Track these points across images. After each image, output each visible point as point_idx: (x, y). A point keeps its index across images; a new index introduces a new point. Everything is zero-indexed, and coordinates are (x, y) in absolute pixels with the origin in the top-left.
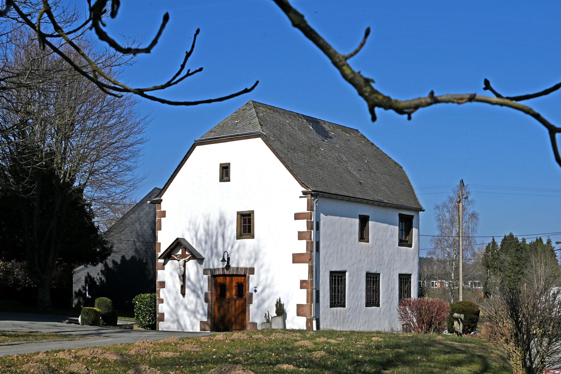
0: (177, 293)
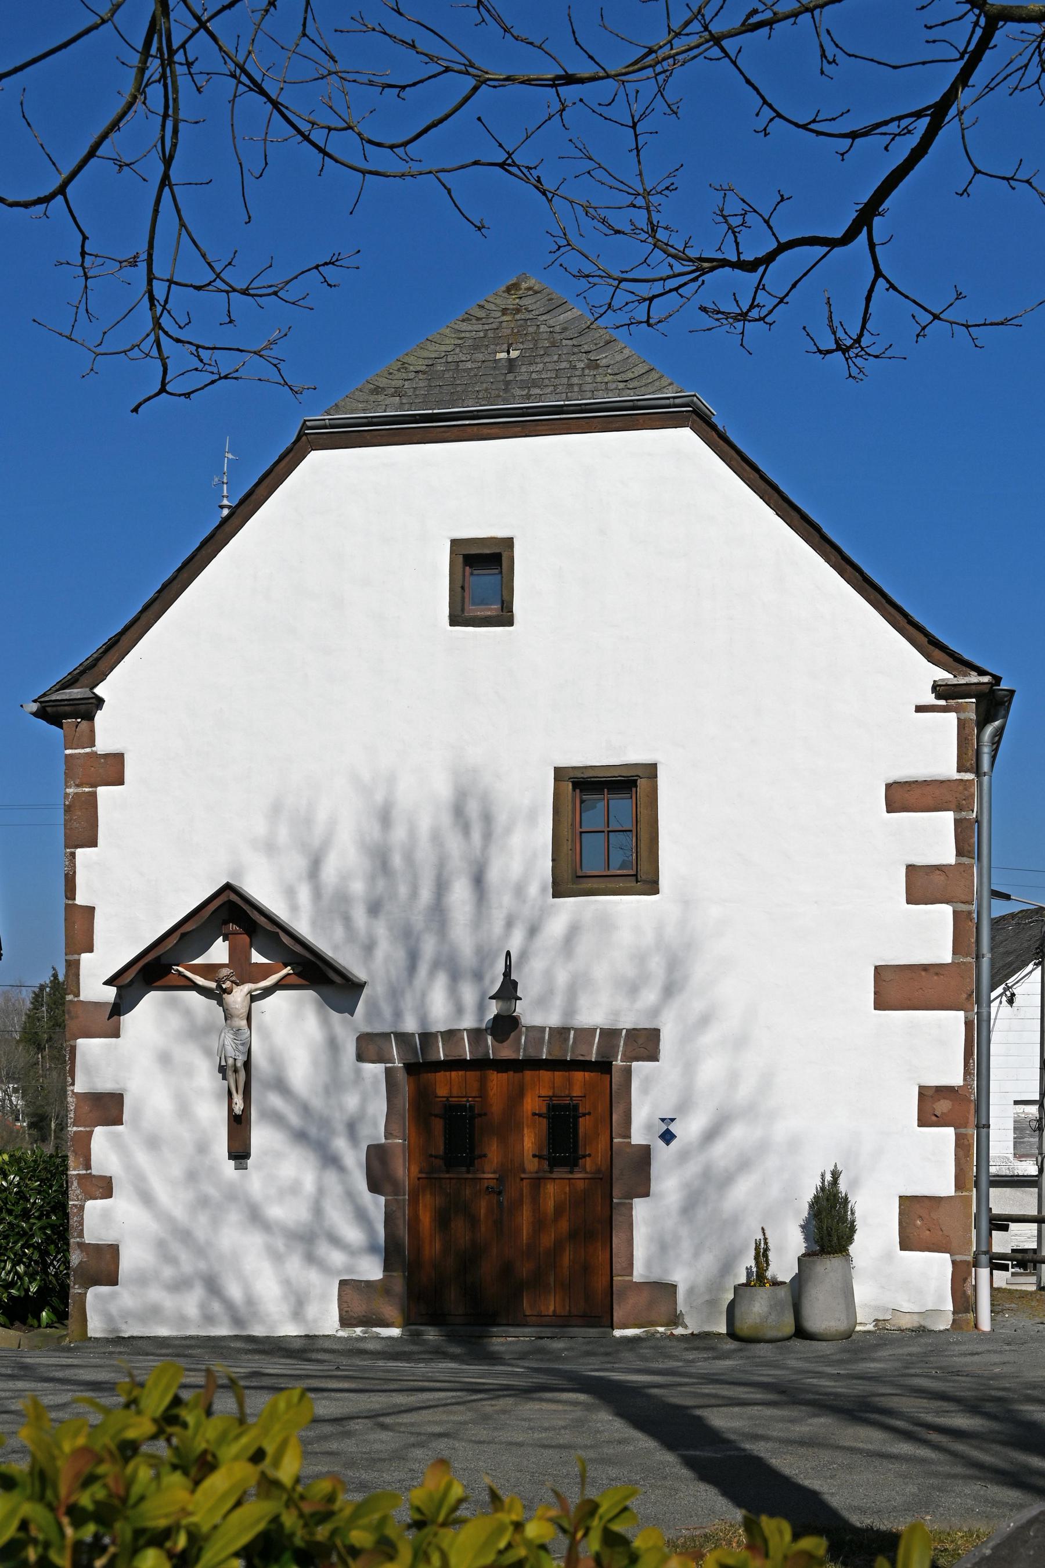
0: (202, 1148)
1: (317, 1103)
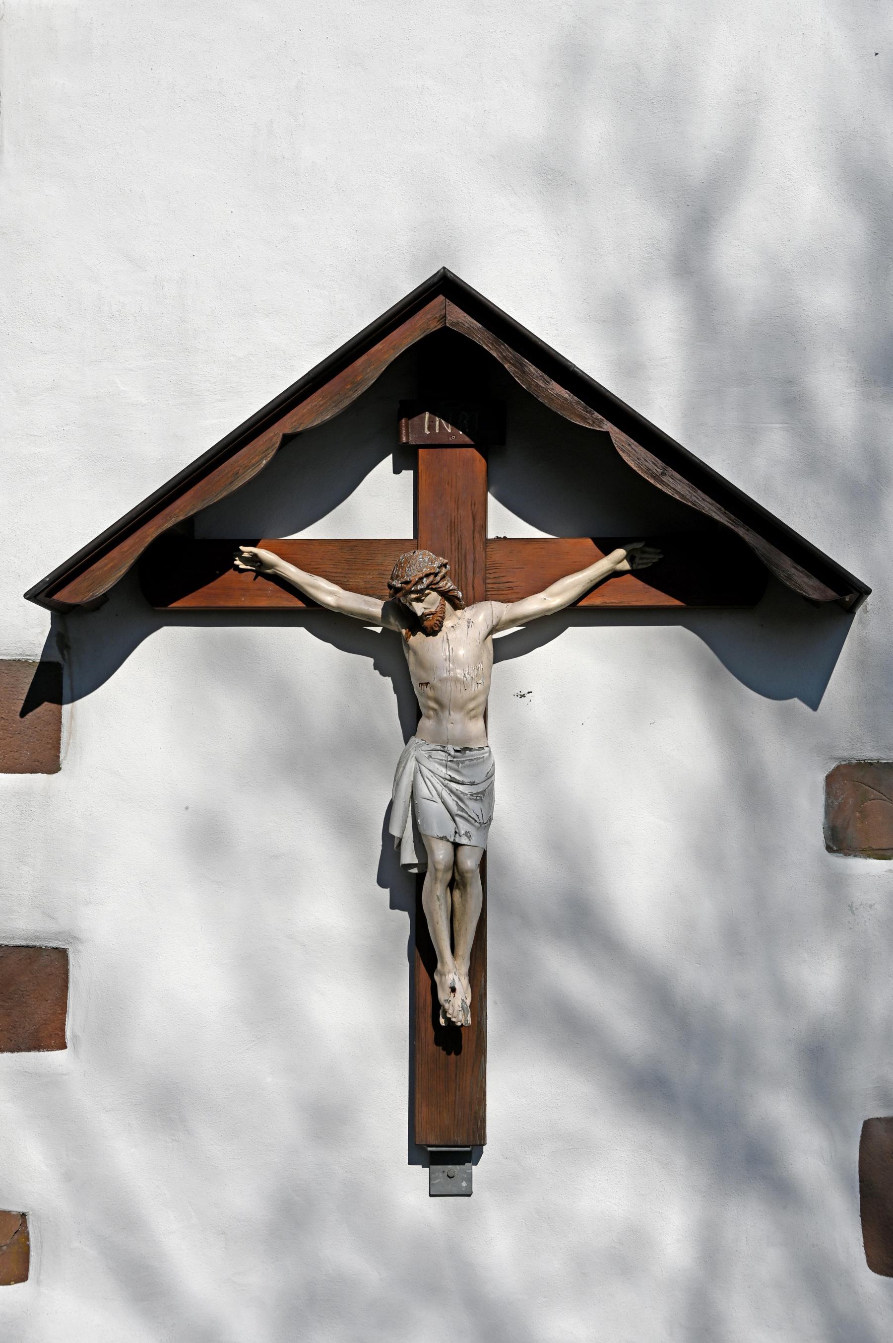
0: (328, 1119)
1: (700, 980)
